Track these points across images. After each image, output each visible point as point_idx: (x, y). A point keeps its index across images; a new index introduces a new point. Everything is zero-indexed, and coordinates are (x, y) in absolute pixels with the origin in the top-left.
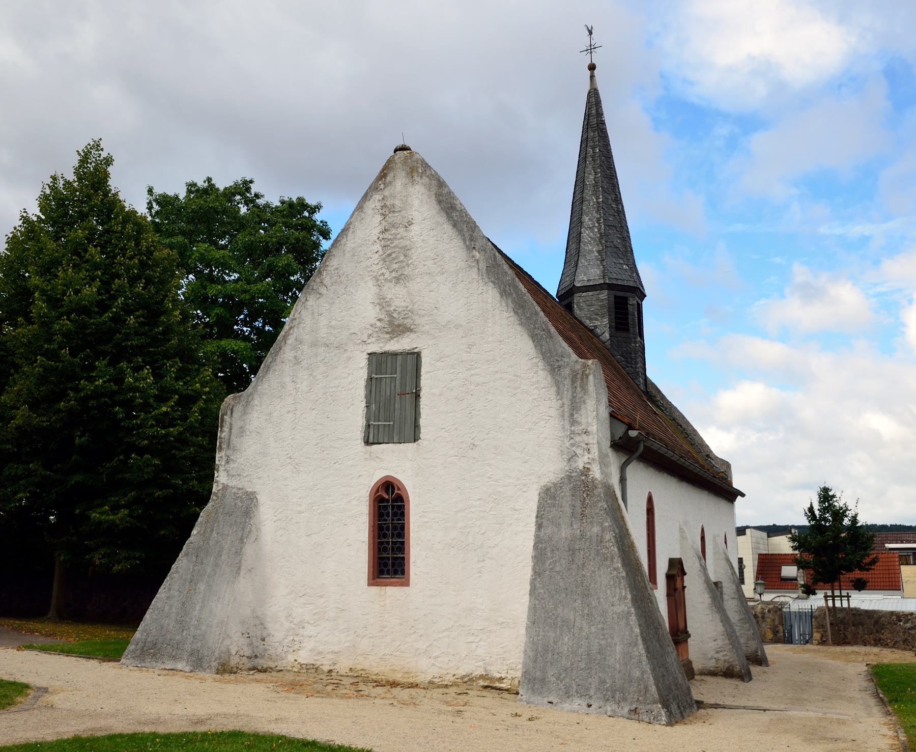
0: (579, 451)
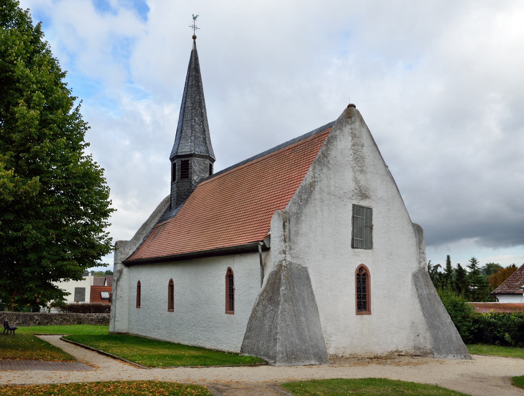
0: (422, 260)
